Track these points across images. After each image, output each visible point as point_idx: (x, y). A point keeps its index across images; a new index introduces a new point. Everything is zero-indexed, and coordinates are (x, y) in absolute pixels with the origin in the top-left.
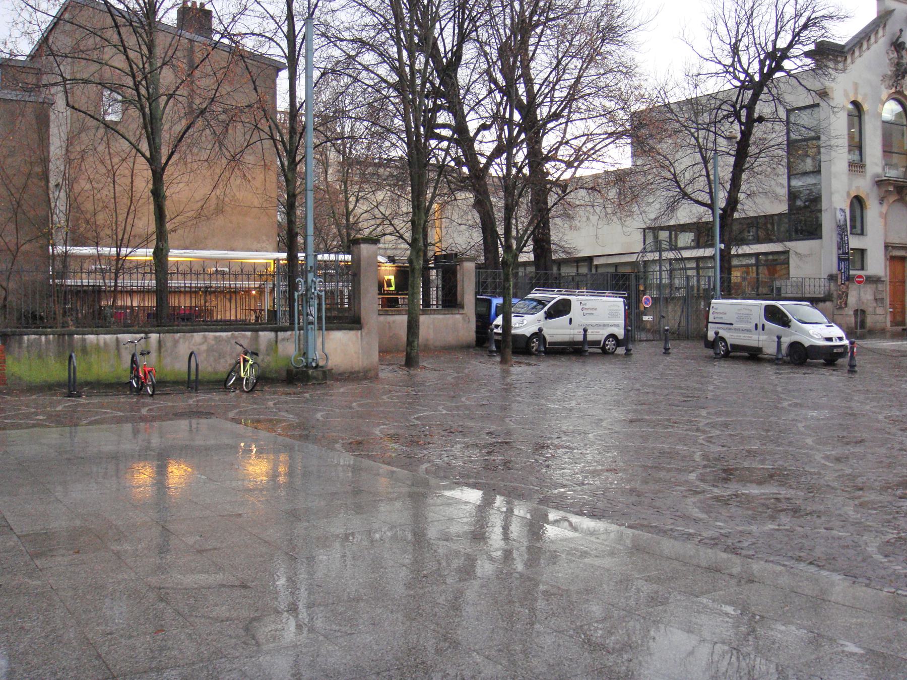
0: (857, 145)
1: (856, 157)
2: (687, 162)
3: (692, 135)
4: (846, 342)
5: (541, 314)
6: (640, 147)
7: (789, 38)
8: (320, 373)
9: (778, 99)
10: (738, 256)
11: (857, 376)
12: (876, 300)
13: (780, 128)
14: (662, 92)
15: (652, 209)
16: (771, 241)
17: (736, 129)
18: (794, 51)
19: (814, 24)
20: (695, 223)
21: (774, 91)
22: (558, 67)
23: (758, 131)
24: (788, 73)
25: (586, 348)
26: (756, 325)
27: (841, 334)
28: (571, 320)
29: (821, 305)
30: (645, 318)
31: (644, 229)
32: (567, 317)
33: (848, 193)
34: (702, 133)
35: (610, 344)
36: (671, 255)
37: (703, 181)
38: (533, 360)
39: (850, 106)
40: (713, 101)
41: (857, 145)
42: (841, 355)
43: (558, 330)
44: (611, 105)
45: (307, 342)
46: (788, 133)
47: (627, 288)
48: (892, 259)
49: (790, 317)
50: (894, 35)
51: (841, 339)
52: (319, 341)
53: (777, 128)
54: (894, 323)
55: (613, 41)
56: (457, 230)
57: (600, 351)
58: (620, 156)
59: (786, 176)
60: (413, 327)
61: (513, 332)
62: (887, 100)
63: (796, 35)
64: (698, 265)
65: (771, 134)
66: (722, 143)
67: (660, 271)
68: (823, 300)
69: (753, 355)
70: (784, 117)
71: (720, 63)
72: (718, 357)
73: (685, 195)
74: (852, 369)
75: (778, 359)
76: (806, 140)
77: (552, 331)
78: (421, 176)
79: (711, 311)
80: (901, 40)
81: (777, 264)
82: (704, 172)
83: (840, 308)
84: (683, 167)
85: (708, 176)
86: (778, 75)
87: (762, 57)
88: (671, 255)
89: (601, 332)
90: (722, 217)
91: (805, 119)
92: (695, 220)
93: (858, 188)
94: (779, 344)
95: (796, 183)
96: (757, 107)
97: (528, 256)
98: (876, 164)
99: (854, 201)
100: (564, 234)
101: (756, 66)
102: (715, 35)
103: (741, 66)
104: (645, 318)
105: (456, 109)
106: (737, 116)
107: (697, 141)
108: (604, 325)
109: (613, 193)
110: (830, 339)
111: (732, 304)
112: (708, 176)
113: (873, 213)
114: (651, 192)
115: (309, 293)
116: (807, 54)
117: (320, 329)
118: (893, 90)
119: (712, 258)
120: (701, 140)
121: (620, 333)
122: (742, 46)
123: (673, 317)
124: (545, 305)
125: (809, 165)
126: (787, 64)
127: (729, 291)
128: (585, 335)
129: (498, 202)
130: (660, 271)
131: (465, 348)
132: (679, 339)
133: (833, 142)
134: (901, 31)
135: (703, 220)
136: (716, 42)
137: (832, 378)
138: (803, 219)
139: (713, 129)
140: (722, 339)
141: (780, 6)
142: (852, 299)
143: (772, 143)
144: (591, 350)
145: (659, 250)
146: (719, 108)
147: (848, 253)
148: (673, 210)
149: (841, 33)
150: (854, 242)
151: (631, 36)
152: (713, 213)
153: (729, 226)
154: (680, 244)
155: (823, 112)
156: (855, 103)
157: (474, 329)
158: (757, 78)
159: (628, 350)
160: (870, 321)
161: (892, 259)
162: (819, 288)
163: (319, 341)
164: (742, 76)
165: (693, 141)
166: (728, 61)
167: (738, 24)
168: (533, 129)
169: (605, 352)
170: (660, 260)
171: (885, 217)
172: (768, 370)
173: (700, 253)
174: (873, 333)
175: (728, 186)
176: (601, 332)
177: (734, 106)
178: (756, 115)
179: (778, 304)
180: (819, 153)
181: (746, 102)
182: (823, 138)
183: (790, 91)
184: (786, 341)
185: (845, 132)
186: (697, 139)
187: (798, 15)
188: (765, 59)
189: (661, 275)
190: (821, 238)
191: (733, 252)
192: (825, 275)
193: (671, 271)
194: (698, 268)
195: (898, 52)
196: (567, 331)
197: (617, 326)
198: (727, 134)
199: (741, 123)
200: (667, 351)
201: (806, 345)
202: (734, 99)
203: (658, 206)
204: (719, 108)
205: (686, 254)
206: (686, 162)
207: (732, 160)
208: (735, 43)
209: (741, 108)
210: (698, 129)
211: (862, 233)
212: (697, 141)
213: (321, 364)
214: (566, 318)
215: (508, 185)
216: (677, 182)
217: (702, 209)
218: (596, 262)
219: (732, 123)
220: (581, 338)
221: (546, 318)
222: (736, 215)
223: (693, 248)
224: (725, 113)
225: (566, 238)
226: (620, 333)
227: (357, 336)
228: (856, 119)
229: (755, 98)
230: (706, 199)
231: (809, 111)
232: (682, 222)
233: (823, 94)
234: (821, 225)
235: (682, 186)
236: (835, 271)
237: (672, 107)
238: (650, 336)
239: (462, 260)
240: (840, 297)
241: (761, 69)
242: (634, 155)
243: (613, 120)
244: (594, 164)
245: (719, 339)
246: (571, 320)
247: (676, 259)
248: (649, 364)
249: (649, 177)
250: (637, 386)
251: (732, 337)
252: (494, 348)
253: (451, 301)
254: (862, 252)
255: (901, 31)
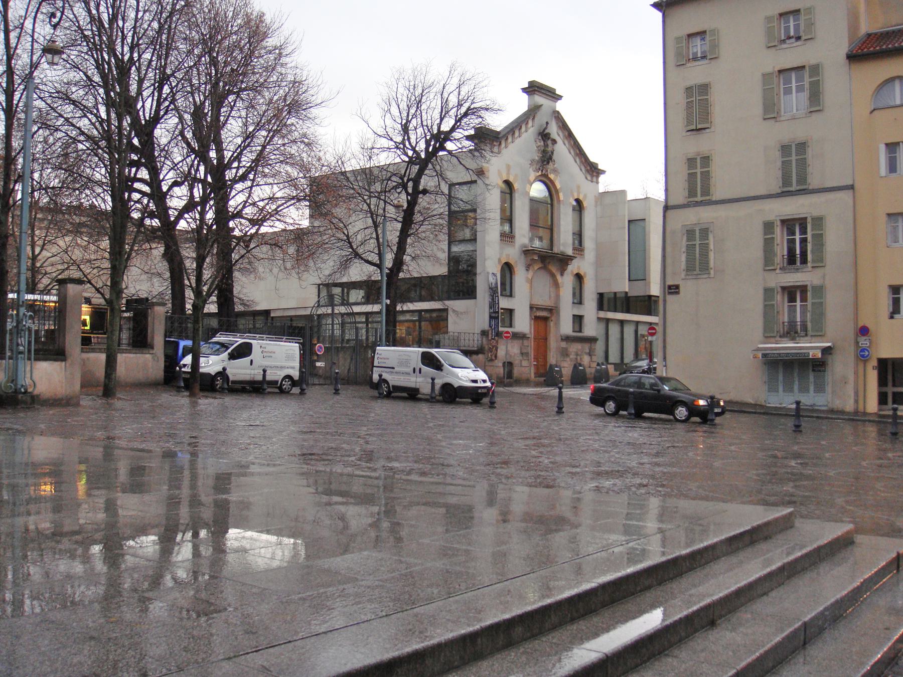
0: (508, 218)
1: (507, 228)
2: (359, 225)
3: (365, 201)
4: (488, 384)
5: (225, 355)
6: (317, 210)
7: (452, 122)
8: (29, 400)
9: (441, 175)
10: (403, 312)
11: (495, 410)
12: (522, 354)
13: (443, 201)
14: (340, 162)
15: (326, 266)
16: (432, 299)
17: (403, 200)
18: (456, 135)
19: (473, 114)
20: (365, 281)
21: (438, 168)
22: (249, 137)
23: (423, 201)
24: (450, 152)
25: (265, 386)
26: (414, 369)
27: (485, 377)
28: (252, 361)
29: (474, 357)
30: (318, 364)
31: (319, 285)
32: (248, 359)
33: (499, 260)
34: (374, 201)
35: (287, 385)
36: (343, 310)
37: (372, 243)
38: (218, 395)
39: (503, 186)
40: (384, 173)
41: (508, 218)
42: (484, 395)
43: (240, 370)
44: (294, 173)
45: (17, 370)
46: (449, 204)
47: (303, 337)
48: (537, 318)
49: (443, 362)
50: (541, 126)
51: (484, 381)
52: (28, 368)
53: (439, 200)
54: (537, 375)
55: (265, 36)
56: (146, 279)
57: (277, 390)
58: (299, 216)
59: (447, 242)
60: (111, 363)
61: (201, 370)
62: (534, 181)
63: (458, 121)
64: (367, 319)
65: (434, 206)
66: (391, 210)
67: (333, 324)
68: (476, 352)
69: (412, 395)
70: (447, 192)
71: (391, 140)
72: (381, 396)
73: (357, 255)
74: (492, 405)
75: (432, 398)
76: (463, 211)
77: (235, 371)
78: (124, 227)
79: (376, 356)
80: (547, 131)
81: (439, 320)
82: (374, 236)
83: (491, 360)
84: (356, 229)
85: (377, 239)
86: (441, 153)
87: (428, 138)
88: (343, 310)
89: (279, 373)
90: (388, 275)
91: (462, 193)
92: (365, 278)
93: (508, 255)
94: (433, 384)
95: (455, 249)
96: (422, 181)
97: (211, 307)
98: (524, 236)
99: (505, 267)
100: (243, 287)
101: (422, 146)
102: (388, 115)
103: (410, 143)
104: (318, 364)
105: (154, 172)
106: (405, 187)
107: (369, 207)
108: (281, 367)
109: (292, 250)
110: (475, 381)
111: (394, 351)
112: (377, 239)
113: (521, 278)
114: (326, 251)
115: (20, 325)
116: (468, 138)
117: (29, 359)
118: (540, 173)
119: (379, 313)
120: (372, 207)
121: (296, 374)
122: (411, 126)
123: (343, 365)
124: (227, 348)
125: (467, 233)
126: (449, 145)
127: (393, 341)
128: (264, 375)
129: (188, 253)
130: (333, 324)
131: (154, 385)
132: (348, 384)
133: (487, 215)
134: (547, 123)
135: (373, 278)
136: (389, 122)
137: (477, 412)
138: (460, 280)
139: (383, 197)
140: (386, 381)
141: (445, 95)
142: (501, 352)
143: (435, 213)
144: (269, 390)
145: (332, 305)
146: (389, 179)
147: (498, 312)
148: (346, 268)
149: (497, 122)
150: (504, 303)
151: (314, 112)
152: (381, 272)
153: (395, 286)
154: (352, 300)
155: (479, 188)
156: (508, 183)
157: (163, 365)
158: (423, 155)
159: (302, 390)
160: (516, 372)
161: (537, 318)
162: (474, 342)
163: (28, 368)
164: (410, 153)
165: (365, 207)
166: (399, 139)
167: (409, 107)
168: (219, 189)
169: (282, 391)
170: (333, 315)
171: (531, 282)
172: (424, 408)
173: (368, 308)
174: (519, 382)
175: (395, 248)
176: (279, 373)
177: (402, 178)
178: (421, 188)
179: (433, 351)
180: (476, 224)
181: (412, 176)
182: (478, 211)
183: (450, 168)
184: (439, 382)
185: (498, 207)
186: (369, 205)
187: (460, 105)
188: (431, 139)
189: (333, 327)
190: (475, 298)
191: (398, 308)
192: (478, 331)
193: (343, 324)
194: (367, 322)
195: (544, 141)
196: (248, 372)
197: (293, 368)
198: (396, 202)
199: (408, 194)
200: (337, 392)
201: (456, 386)
202: (403, 172)
203: (332, 264)
204: (389, 179)
205: (357, 309)
206: (358, 225)
207: (399, 226)
208: (406, 124)
209: (408, 180)
210: (370, 197)
211: (511, 296)
212: (369, 207)
213: (30, 390)
214: (247, 360)
215: (199, 238)
216: (350, 243)
217: (372, 268)
218: (272, 315)
219: (399, 193)
220: (260, 378)
221: (229, 359)
222: (401, 275)
223: (363, 304)
224: (395, 184)
225: (245, 291)
226: (296, 374)
227: (61, 368)
228: (508, 196)
229: (420, 173)
230: (375, 258)
231: (465, 187)
232: (353, 280)
233: (481, 173)
234: (475, 287)
235: (355, 247)
236: (486, 327)
237: (348, 175)
238: (322, 381)
239: (153, 304)
240: (490, 350)
241: (427, 149)
242: (311, 216)
243: (296, 187)
244: (277, 223)
245: (383, 381)
246: (252, 361)
247: (348, 314)
248: (320, 403)
249: (325, 238)
250: (311, 413)
251: (394, 380)
252: (182, 385)
253: (141, 342)
254: (511, 312)
255: (547, 123)
